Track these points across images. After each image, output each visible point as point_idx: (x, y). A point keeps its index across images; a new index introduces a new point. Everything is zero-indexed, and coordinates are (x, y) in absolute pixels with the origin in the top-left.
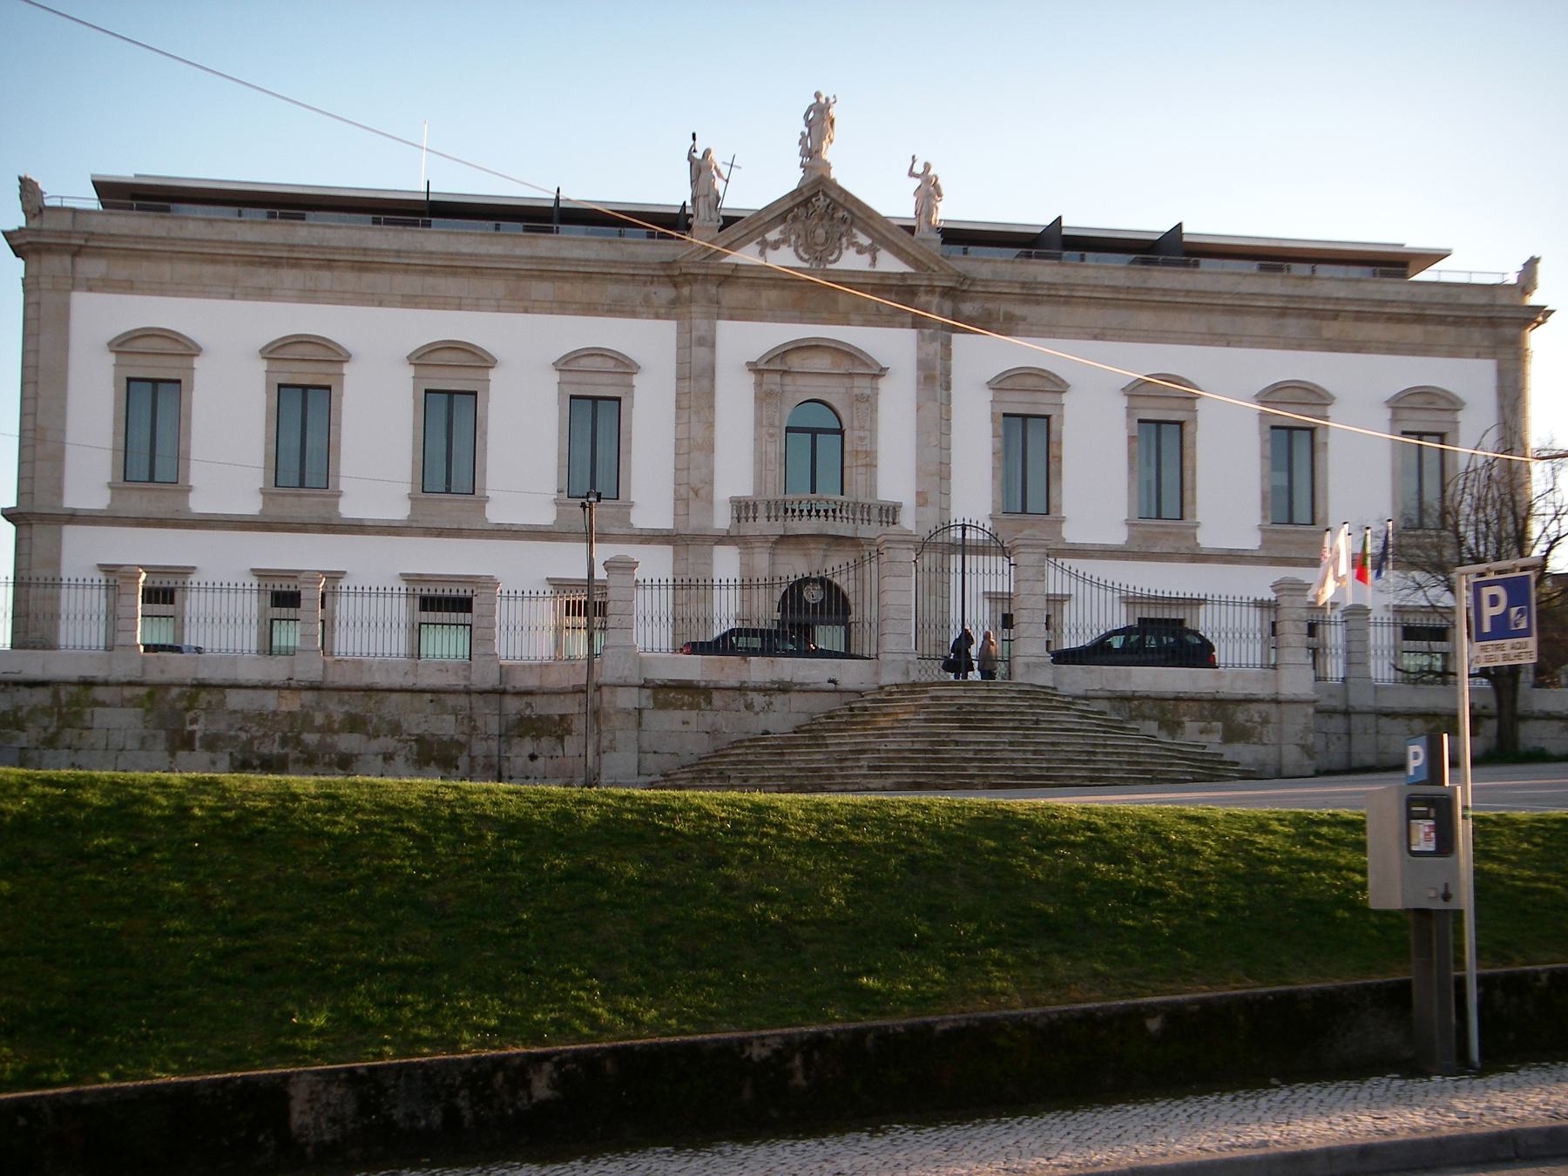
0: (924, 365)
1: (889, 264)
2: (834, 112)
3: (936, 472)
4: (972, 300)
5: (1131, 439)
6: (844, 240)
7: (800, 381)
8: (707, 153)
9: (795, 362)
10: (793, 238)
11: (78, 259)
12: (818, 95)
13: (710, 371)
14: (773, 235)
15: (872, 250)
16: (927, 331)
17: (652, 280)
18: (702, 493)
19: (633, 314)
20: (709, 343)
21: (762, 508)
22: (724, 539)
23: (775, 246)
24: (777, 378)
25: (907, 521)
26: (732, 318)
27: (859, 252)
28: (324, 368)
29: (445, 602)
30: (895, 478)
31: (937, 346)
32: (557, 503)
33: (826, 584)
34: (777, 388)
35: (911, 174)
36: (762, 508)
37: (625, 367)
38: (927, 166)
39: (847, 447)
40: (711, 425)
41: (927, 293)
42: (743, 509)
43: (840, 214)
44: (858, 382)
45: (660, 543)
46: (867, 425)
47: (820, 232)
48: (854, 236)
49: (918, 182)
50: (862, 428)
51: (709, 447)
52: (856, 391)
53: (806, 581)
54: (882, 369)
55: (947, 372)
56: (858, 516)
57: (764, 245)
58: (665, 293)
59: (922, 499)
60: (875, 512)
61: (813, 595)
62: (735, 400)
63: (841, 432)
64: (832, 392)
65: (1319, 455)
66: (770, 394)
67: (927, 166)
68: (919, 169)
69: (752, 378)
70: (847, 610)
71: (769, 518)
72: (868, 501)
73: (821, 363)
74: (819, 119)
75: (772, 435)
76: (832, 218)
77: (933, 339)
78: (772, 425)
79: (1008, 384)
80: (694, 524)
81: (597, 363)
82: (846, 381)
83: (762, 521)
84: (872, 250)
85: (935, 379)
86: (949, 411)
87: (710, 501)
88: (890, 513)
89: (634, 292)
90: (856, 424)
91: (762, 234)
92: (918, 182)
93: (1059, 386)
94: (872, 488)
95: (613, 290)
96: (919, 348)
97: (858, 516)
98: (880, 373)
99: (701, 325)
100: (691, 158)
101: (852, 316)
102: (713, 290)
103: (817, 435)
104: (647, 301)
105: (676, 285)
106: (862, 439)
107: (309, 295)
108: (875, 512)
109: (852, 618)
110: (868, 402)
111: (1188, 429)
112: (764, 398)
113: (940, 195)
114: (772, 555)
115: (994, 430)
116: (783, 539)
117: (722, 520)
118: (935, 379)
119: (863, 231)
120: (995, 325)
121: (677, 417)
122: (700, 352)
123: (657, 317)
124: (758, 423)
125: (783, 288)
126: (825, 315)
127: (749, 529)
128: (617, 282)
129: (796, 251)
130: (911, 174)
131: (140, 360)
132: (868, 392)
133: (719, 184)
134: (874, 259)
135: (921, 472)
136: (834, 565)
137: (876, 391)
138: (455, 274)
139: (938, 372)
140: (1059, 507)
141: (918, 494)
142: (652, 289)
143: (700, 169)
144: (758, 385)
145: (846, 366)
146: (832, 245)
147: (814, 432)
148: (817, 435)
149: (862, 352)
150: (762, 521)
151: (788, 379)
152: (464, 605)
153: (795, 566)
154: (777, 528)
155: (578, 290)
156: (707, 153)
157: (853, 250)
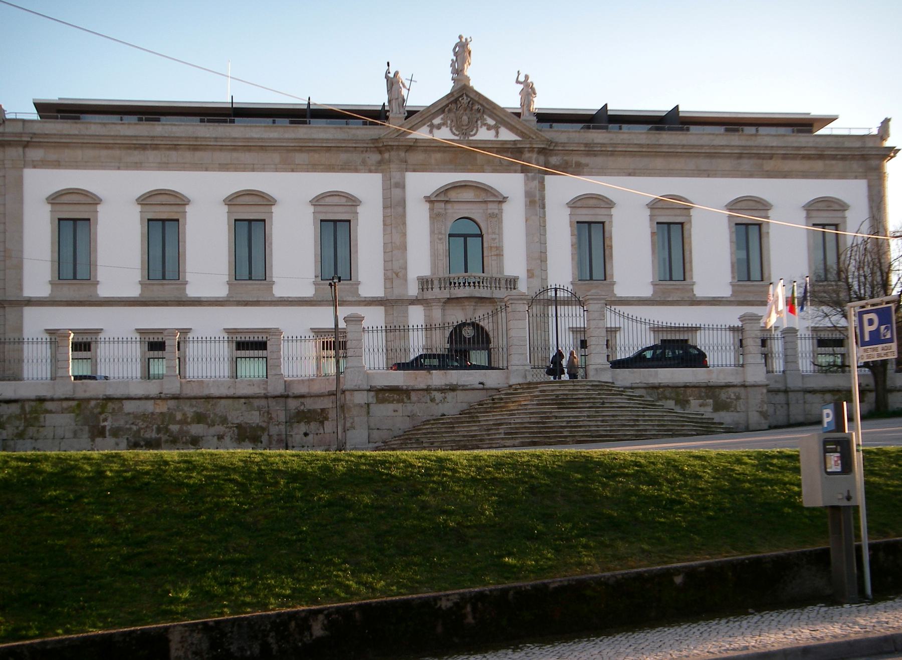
0: (529, 195)
1: (506, 135)
2: (470, 47)
3: (538, 258)
4: (556, 155)
5: (653, 234)
6: (479, 122)
7: (456, 206)
8: (396, 74)
9: (453, 195)
10: (449, 122)
11: (27, 149)
12: (460, 37)
13: (402, 203)
14: (437, 121)
15: (496, 128)
16: (530, 175)
17: (366, 150)
18: (400, 274)
19: (356, 170)
20: (402, 186)
21: (436, 282)
22: (414, 302)
23: (439, 127)
24: (442, 205)
25: (522, 287)
26: (414, 171)
27: (488, 129)
28: (175, 208)
29: (251, 344)
30: (514, 262)
31: (536, 183)
32: (315, 284)
33: (475, 326)
34: (442, 211)
35: (518, 82)
36: (436, 282)
37: (353, 202)
38: (527, 77)
39: (485, 245)
40: (404, 235)
41: (529, 152)
42: (425, 283)
43: (476, 107)
44: (490, 206)
45: (377, 305)
46: (497, 231)
47: (465, 118)
48: (485, 120)
49: (521, 87)
50: (494, 233)
51: (404, 247)
52: (489, 211)
53: (464, 324)
54: (504, 198)
55: (543, 198)
56: (493, 285)
57: (432, 127)
58: (375, 157)
59: (530, 274)
60: (503, 282)
61: (468, 333)
62: (418, 219)
63: (481, 236)
64: (476, 212)
65: (764, 240)
66: (438, 215)
67: (527, 77)
68: (522, 79)
69: (427, 205)
70: (488, 341)
71: (440, 288)
72: (499, 276)
73: (468, 195)
74: (462, 51)
75: (440, 239)
76: (472, 110)
77: (534, 179)
78: (440, 233)
79: (579, 204)
80: (397, 293)
81: (336, 200)
82: (483, 206)
83: (436, 290)
84: (496, 128)
85: (536, 202)
86: (545, 221)
87: (405, 279)
88: (512, 282)
89: (356, 157)
90: (490, 230)
91: (431, 120)
92: (521, 87)
93: (609, 204)
94: (501, 267)
95: (344, 157)
96: (526, 184)
97: (493, 285)
98: (502, 200)
99: (396, 176)
100: (387, 77)
101: (485, 167)
102: (402, 154)
103: (468, 239)
104: (364, 162)
105: (380, 152)
106: (494, 239)
107: (164, 166)
108: (503, 282)
109: (491, 346)
110: (497, 217)
111: (686, 227)
112: (435, 217)
113: (535, 94)
114: (443, 310)
115: (572, 231)
116: (450, 300)
117: (413, 290)
118: (536, 202)
119: (490, 116)
120: (570, 169)
121: (384, 230)
122: (396, 192)
123: (370, 171)
124: (432, 232)
125: (444, 152)
126: (469, 167)
127: (429, 295)
128: (346, 151)
129: (451, 130)
130: (518, 82)
131: (65, 208)
132: (496, 211)
133: (404, 92)
134: (497, 133)
135: (529, 258)
136: (480, 315)
137: (501, 211)
138: (249, 151)
139: (537, 199)
140: (612, 275)
141: (528, 271)
142: (366, 155)
143: (393, 83)
144: (431, 209)
145: (483, 197)
146: (472, 125)
147: (465, 236)
148: (468, 239)
149: (492, 188)
150: (436, 290)
151: (449, 206)
152: (262, 346)
153: (457, 316)
154: (446, 294)
155: (324, 158)
156: (396, 74)
157: (484, 128)
